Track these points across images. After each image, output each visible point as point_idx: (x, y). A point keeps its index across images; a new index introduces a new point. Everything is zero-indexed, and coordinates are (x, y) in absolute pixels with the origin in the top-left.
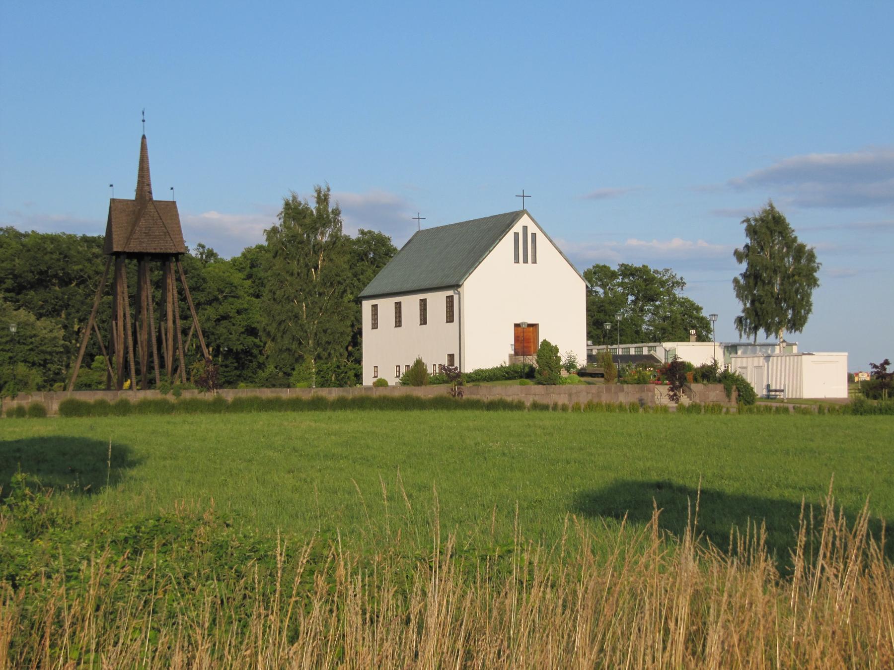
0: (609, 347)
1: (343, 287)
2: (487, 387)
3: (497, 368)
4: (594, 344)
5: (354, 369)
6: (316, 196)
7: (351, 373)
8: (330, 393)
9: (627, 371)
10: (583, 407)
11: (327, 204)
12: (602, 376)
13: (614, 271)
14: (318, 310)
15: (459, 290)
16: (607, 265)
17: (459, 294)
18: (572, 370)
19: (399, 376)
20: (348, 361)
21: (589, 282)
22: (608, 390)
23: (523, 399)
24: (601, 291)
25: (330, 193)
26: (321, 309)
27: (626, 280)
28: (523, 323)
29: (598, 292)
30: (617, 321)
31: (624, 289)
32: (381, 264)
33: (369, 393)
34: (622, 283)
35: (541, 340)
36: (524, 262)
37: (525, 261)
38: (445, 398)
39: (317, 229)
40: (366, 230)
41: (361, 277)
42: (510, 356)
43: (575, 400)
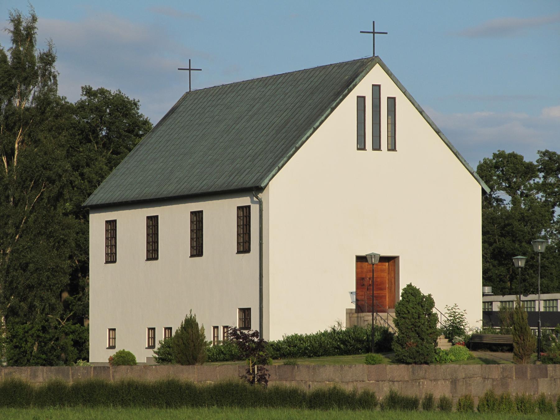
0: (523, 298)
1: (56, 190)
2: (308, 367)
3: (325, 334)
4: (495, 293)
5: (73, 332)
6: (12, 29)
7: (68, 341)
8: (35, 376)
9: (554, 339)
10: (476, 403)
11: (32, 45)
12: (510, 348)
13: (531, 164)
14: (11, 231)
15: (260, 195)
16: (518, 152)
17: (260, 203)
18: (457, 338)
19: (153, 347)
20: (62, 319)
21: (487, 182)
22: (521, 374)
23: (372, 389)
24: (507, 198)
25: (36, 25)
26: (18, 227)
27: (551, 180)
28: (372, 256)
29: (501, 200)
30: (537, 254)
31: (549, 195)
32: (122, 149)
33: (102, 377)
34: (544, 184)
35: (403, 286)
36: (374, 149)
37: (377, 147)
38: (237, 385)
39: (13, 88)
40: (95, 88)
41: (86, 170)
42: (349, 313)
43: (462, 391)
